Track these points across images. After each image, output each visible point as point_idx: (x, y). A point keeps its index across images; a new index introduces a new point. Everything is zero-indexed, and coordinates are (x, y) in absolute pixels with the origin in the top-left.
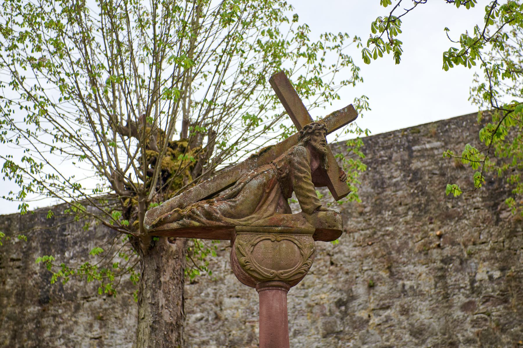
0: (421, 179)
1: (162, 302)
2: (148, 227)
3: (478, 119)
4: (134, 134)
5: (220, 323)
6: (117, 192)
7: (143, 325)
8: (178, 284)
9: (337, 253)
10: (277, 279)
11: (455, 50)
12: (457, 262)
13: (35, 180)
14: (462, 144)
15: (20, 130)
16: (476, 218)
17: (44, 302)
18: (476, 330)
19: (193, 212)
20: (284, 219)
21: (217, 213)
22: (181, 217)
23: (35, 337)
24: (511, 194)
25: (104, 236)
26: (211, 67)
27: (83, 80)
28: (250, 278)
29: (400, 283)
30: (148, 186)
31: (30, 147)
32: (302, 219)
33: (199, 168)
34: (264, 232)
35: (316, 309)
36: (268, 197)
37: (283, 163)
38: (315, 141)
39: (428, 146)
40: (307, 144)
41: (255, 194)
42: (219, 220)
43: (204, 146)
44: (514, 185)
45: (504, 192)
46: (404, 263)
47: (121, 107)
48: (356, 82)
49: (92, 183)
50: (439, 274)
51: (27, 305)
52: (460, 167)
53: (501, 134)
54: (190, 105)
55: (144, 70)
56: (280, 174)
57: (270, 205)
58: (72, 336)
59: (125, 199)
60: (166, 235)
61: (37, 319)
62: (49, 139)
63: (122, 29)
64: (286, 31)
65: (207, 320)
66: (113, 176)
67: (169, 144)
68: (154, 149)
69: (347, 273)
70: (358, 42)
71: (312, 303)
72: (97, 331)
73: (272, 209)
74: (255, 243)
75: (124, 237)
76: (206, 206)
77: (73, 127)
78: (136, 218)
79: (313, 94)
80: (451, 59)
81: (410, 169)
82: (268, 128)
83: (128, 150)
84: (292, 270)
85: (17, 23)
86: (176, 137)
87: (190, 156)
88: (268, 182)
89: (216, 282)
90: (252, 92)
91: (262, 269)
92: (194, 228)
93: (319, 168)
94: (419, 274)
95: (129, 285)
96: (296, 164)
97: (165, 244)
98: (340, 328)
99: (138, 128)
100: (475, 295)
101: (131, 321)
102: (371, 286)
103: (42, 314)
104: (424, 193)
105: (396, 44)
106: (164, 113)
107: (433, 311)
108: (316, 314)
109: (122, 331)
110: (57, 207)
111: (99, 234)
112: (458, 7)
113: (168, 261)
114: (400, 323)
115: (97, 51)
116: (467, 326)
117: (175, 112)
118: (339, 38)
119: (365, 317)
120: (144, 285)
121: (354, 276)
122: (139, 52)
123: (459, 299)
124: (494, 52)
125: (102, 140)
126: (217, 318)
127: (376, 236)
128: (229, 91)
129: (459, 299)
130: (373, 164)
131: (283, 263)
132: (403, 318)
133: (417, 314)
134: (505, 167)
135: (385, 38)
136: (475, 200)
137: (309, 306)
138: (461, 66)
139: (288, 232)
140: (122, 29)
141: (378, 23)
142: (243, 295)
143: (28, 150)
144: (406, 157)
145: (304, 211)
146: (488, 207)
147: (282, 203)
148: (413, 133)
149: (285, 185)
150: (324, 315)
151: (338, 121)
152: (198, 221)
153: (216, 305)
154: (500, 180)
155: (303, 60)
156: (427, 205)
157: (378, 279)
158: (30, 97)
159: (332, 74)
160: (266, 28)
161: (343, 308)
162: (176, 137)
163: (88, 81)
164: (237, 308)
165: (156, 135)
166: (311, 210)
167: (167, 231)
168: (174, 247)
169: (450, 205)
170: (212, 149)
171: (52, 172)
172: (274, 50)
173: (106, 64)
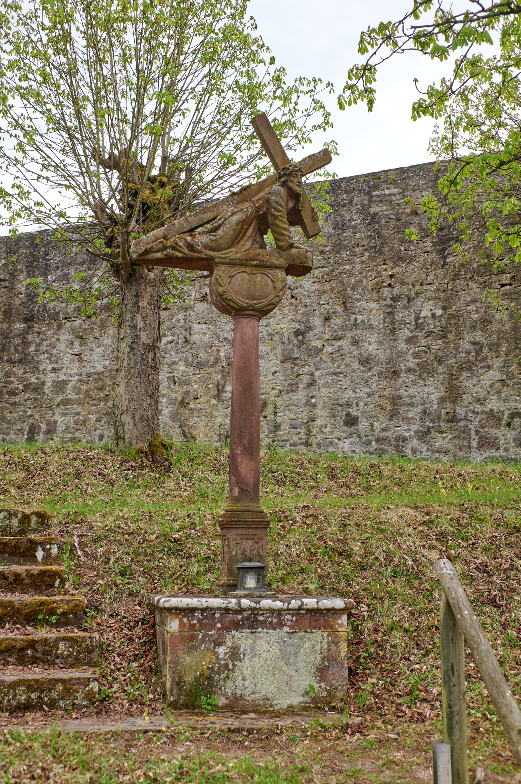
0: (378, 222)
1: (140, 325)
2: (134, 256)
3: (435, 169)
4: (117, 166)
5: (189, 346)
6: (100, 221)
7: (123, 344)
9: (297, 288)
11: (424, 101)
13: (24, 206)
14: (418, 192)
15: (9, 158)
16: (425, 261)
17: (29, 319)
18: (417, 361)
19: (177, 244)
20: (259, 254)
22: (165, 248)
23: (21, 351)
24: (458, 240)
25: (84, 262)
26: (192, 105)
27: (69, 111)
28: (228, 307)
29: (353, 316)
30: (129, 217)
31: (19, 174)
32: (276, 254)
33: (178, 203)
34: (241, 265)
35: (276, 338)
36: (246, 232)
37: (261, 202)
38: (292, 182)
39: (387, 192)
40: (284, 184)
41: (234, 230)
42: (200, 252)
43: (181, 182)
44: (461, 232)
45: (452, 239)
46: (357, 300)
47: (103, 140)
48: (327, 127)
49: (76, 212)
50: (389, 310)
51: (14, 322)
52: (415, 213)
53: (458, 184)
54: (169, 143)
55: (127, 106)
57: (247, 240)
58: (54, 352)
59: (107, 228)
60: (145, 263)
61: (23, 335)
62: (37, 168)
63: (107, 63)
64: (262, 73)
65: (177, 343)
66: (96, 206)
67: (149, 179)
68: (135, 183)
69: (306, 306)
70: (330, 87)
71: (273, 332)
72: (77, 348)
73: (249, 244)
75: (105, 265)
76: (189, 238)
77: (57, 156)
78: (118, 247)
79: (286, 137)
80: (419, 110)
81: (369, 213)
82: (242, 167)
83: (110, 183)
84: (266, 301)
85: (5, 51)
86: (155, 172)
87: (168, 191)
89: (186, 309)
90: (228, 133)
92: (177, 258)
93: (294, 208)
94: (371, 310)
95: (108, 308)
99: (121, 162)
100: (418, 330)
101: (107, 341)
102: (327, 319)
103: (28, 330)
104: (380, 236)
105: (370, 92)
106: (147, 148)
107: (380, 343)
108: (276, 341)
109: (100, 350)
110: (40, 232)
111: (80, 260)
112: (432, 58)
114: (350, 352)
115: (81, 83)
116: (410, 357)
117: (155, 150)
118: (312, 82)
119: (320, 346)
122: (123, 87)
123: (405, 333)
124: (455, 105)
125: (86, 172)
126: (186, 341)
127: (333, 274)
128: (206, 129)
129: (405, 333)
130: (336, 205)
132: (354, 348)
133: (366, 345)
134: (456, 215)
135: (360, 86)
136: (425, 244)
137: (270, 334)
138: (428, 117)
139: (263, 266)
140: (107, 63)
141: (355, 71)
142: (211, 322)
143: (17, 177)
144: (366, 202)
145: (278, 247)
146: (437, 252)
147: (258, 239)
148: (374, 179)
149: (262, 222)
150: (283, 343)
151: (313, 164)
152: (181, 252)
153: (186, 330)
154: (450, 226)
155: (278, 103)
156: (381, 247)
157: (333, 313)
158: (18, 126)
159: (305, 118)
160: (245, 69)
161: (300, 337)
162: (155, 172)
163: (73, 112)
164: (204, 334)
165: (136, 168)
166: (284, 246)
167: (152, 260)
168: (152, 275)
169: (402, 248)
170: (189, 185)
171: (40, 199)
172: (251, 92)
173: (91, 98)
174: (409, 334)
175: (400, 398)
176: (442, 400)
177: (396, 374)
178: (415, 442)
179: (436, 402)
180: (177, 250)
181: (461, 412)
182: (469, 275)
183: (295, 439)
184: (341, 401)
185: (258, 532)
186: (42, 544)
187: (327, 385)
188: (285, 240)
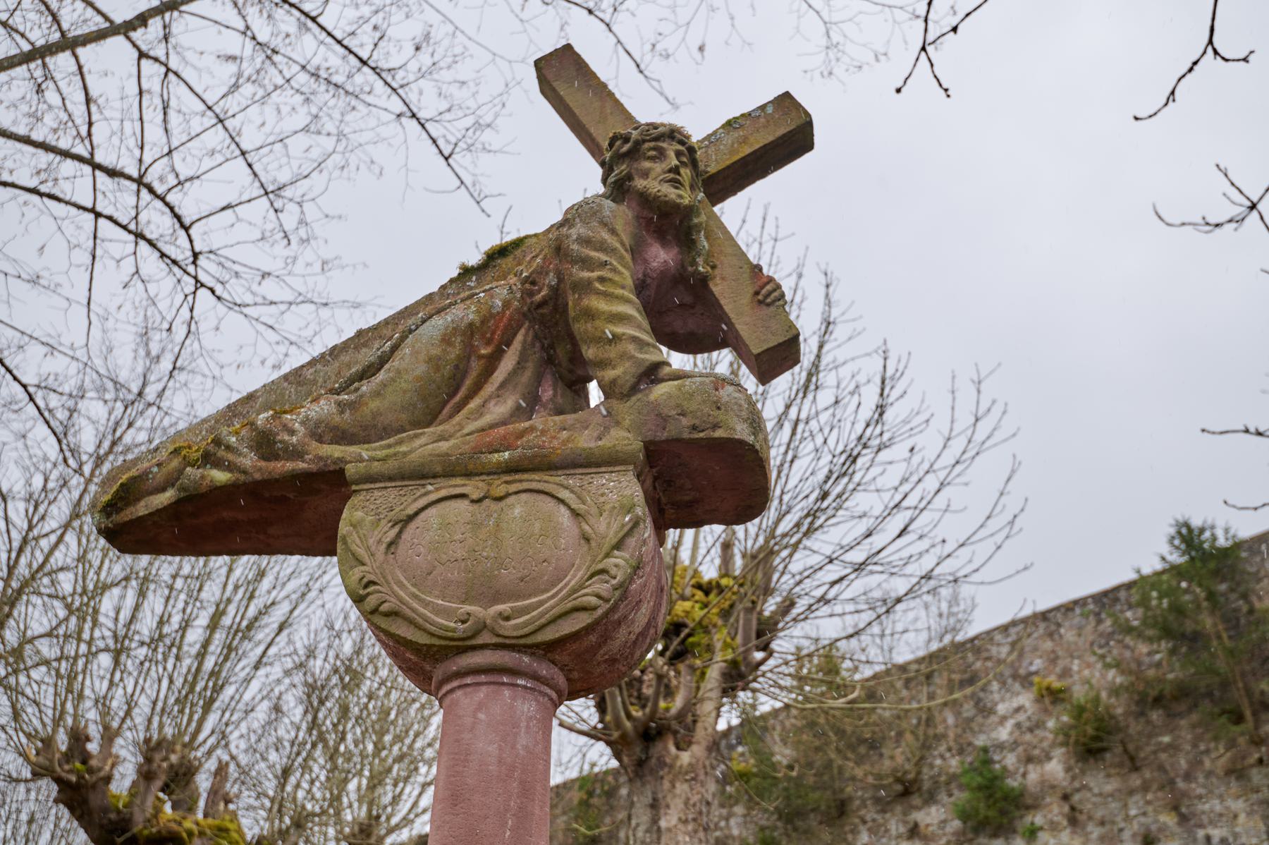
8: (696, 831)
9: (1078, 790)
10: (485, 638)
21: (292, 432)
29: (1201, 833)
38: (645, 174)
42: (297, 454)
46: (1200, 797)
56: (531, 294)
74: (410, 511)
91: (426, 604)
96: (575, 247)
97: (668, 752)
113: (674, 787)
120: (631, 838)
121: (1115, 828)
131: (508, 575)
152: (230, 467)
180: (218, 464)
188: (624, 356)
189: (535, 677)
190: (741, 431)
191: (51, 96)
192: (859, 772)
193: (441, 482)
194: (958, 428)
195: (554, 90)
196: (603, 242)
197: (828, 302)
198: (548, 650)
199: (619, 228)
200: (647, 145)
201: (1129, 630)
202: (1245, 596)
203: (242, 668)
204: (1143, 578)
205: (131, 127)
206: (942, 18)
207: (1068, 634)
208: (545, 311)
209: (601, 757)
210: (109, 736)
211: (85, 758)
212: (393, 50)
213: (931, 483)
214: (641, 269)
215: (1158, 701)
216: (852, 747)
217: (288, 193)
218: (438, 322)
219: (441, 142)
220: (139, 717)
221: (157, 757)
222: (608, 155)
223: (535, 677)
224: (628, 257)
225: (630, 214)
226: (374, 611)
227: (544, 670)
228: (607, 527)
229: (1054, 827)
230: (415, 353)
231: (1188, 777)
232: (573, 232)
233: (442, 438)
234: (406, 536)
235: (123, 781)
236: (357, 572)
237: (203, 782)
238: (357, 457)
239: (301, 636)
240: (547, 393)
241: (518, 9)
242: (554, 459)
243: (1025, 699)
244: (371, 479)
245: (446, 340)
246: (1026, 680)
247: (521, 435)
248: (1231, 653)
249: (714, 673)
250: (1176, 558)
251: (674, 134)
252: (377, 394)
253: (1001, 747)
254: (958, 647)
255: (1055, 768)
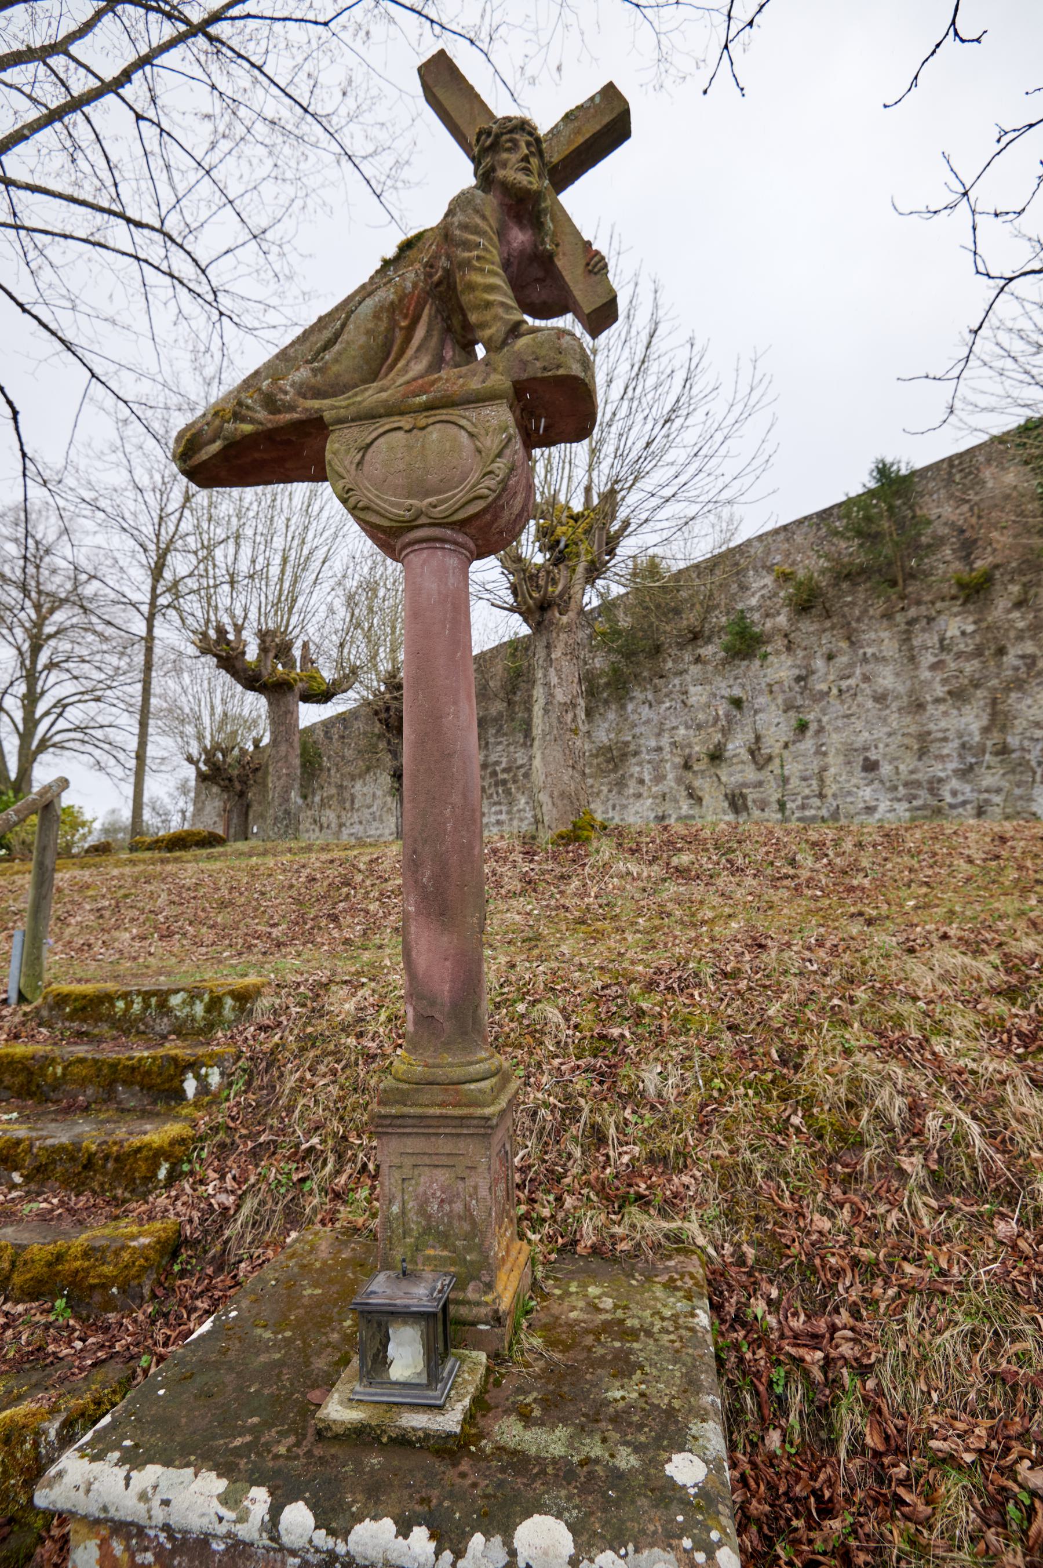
1: (554, 680)
10: (423, 520)
12: (924, 622)
21: (286, 393)
34: (389, 414)
38: (504, 165)
41: (369, 332)
42: (291, 408)
56: (430, 275)
57: (415, 357)
88: (401, 300)
91: (385, 501)
96: (457, 232)
98: (799, 702)
107: (897, 675)
131: (433, 479)
146: (960, 559)
152: (252, 421)
174: (933, 659)
175: (929, 733)
176: (986, 730)
177: (920, 706)
178: (955, 783)
179: (977, 733)
180: (243, 420)
181: (1013, 741)
182: (1007, 578)
183: (807, 791)
184: (856, 746)
185: (462, 1145)
186: (193, 1065)
187: (837, 729)
188: (496, 318)
189: (455, 543)
190: (576, 370)
191: (82, 163)
192: (668, 628)
193: (384, 420)
194: (739, 397)
195: (434, 96)
196: (477, 226)
197: (656, 307)
198: (462, 525)
199: (488, 213)
200: (505, 137)
201: (836, 533)
202: (911, 508)
203: (305, 585)
204: (850, 499)
205: (145, 185)
206: (742, 13)
207: (798, 539)
208: (442, 288)
209: (518, 627)
210: (239, 629)
211: (228, 643)
212: (326, 97)
213: (719, 437)
214: (505, 249)
215: (848, 576)
216: (665, 615)
217: (268, 235)
218: (369, 302)
219: (373, 183)
220: (253, 615)
221: (268, 639)
222: (476, 150)
223: (455, 543)
224: (495, 238)
225: (495, 202)
226: (355, 508)
227: (461, 538)
228: (491, 443)
229: (778, 653)
230: (357, 327)
231: (859, 620)
232: (456, 220)
233: (382, 390)
234: (367, 457)
235: (252, 653)
236: (341, 484)
237: (297, 653)
238: (327, 407)
239: (337, 565)
240: (448, 354)
241: (415, 44)
242: (456, 398)
243: (768, 580)
244: (340, 421)
245: (376, 316)
246: (769, 569)
247: (433, 383)
248: (897, 544)
249: (580, 569)
250: (872, 485)
251: (524, 126)
252: (336, 361)
253: (751, 609)
254: (730, 551)
255: (782, 620)
